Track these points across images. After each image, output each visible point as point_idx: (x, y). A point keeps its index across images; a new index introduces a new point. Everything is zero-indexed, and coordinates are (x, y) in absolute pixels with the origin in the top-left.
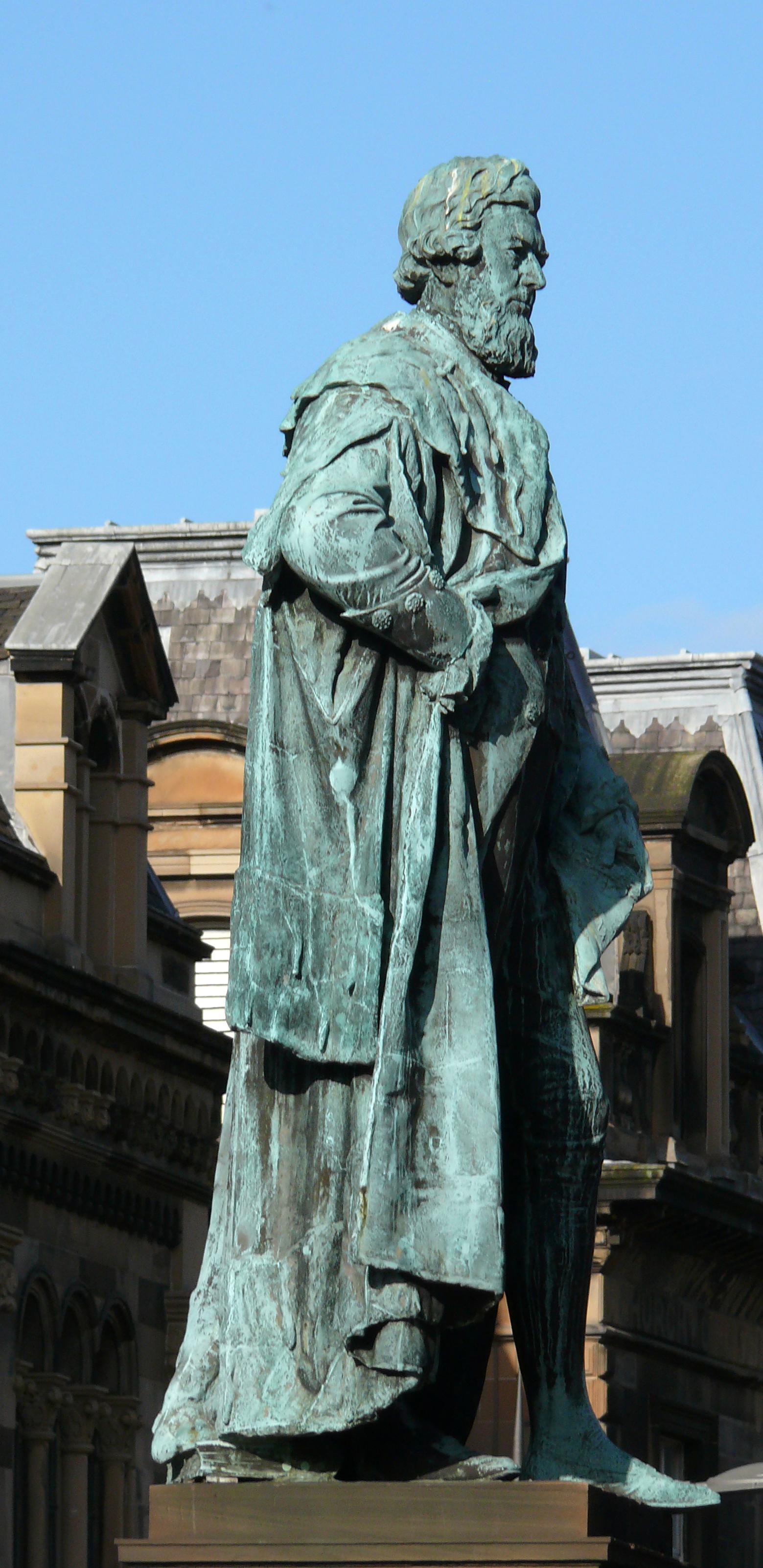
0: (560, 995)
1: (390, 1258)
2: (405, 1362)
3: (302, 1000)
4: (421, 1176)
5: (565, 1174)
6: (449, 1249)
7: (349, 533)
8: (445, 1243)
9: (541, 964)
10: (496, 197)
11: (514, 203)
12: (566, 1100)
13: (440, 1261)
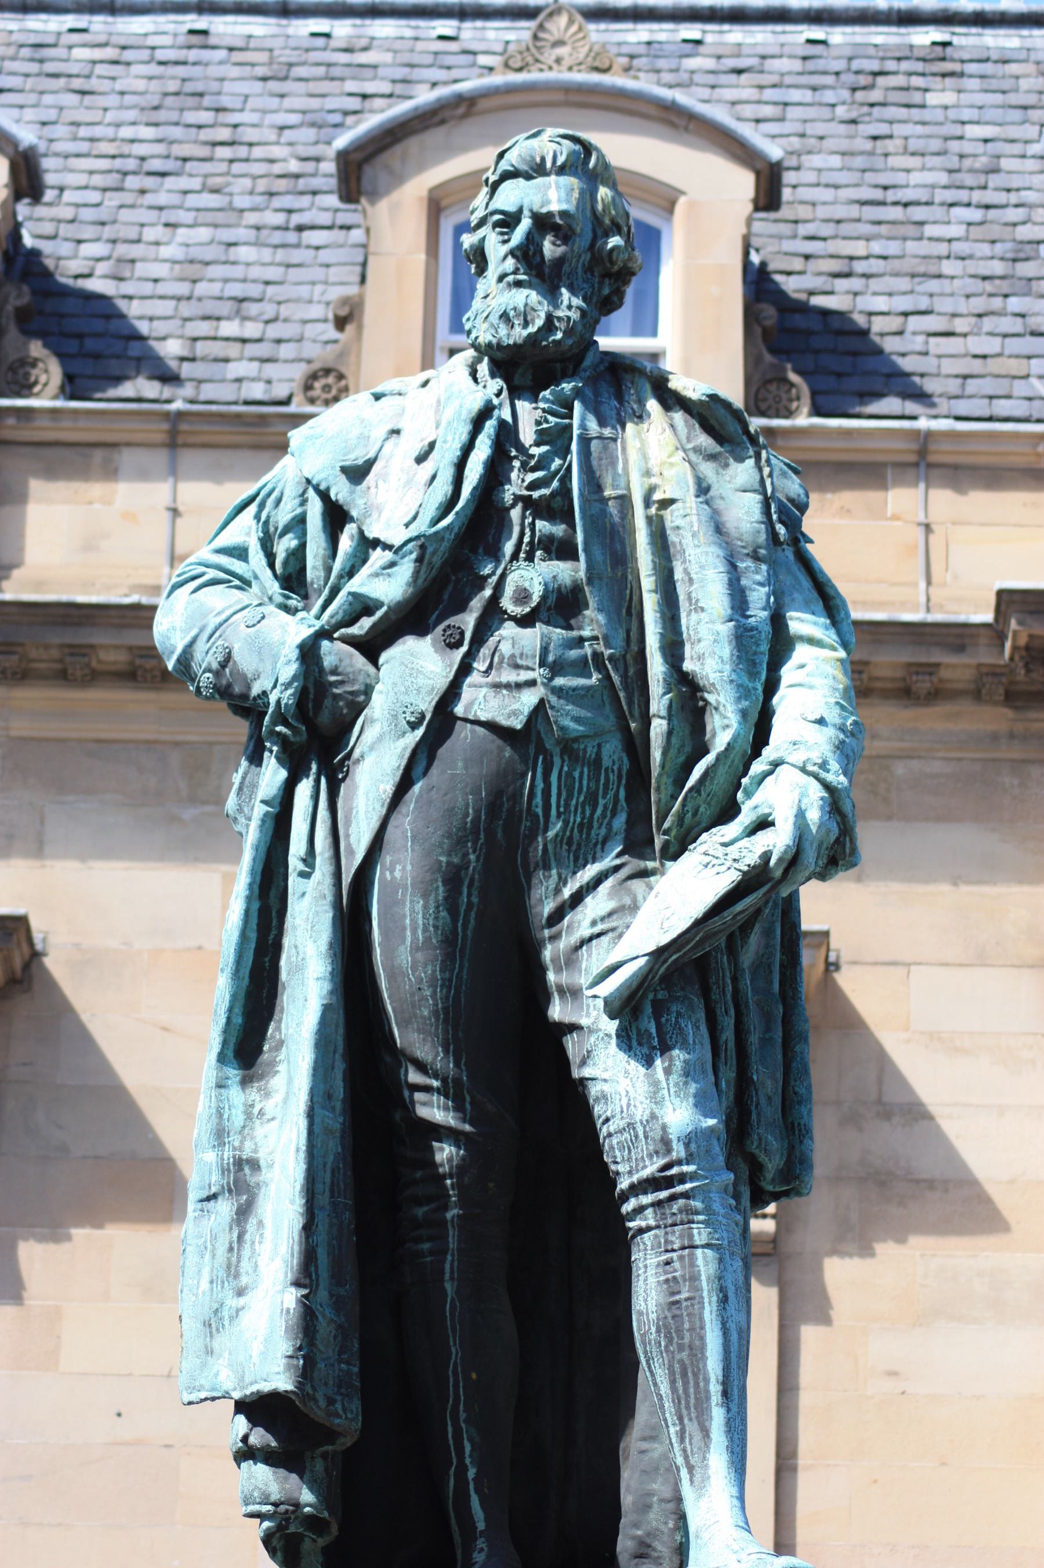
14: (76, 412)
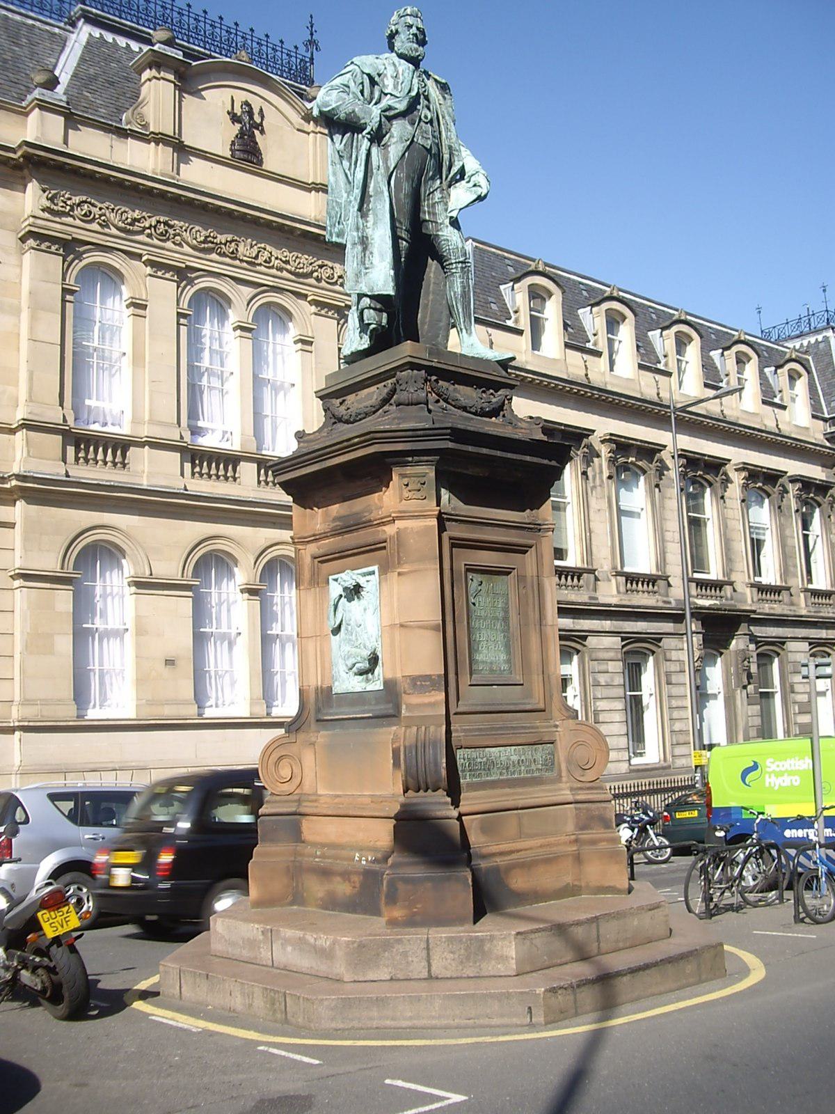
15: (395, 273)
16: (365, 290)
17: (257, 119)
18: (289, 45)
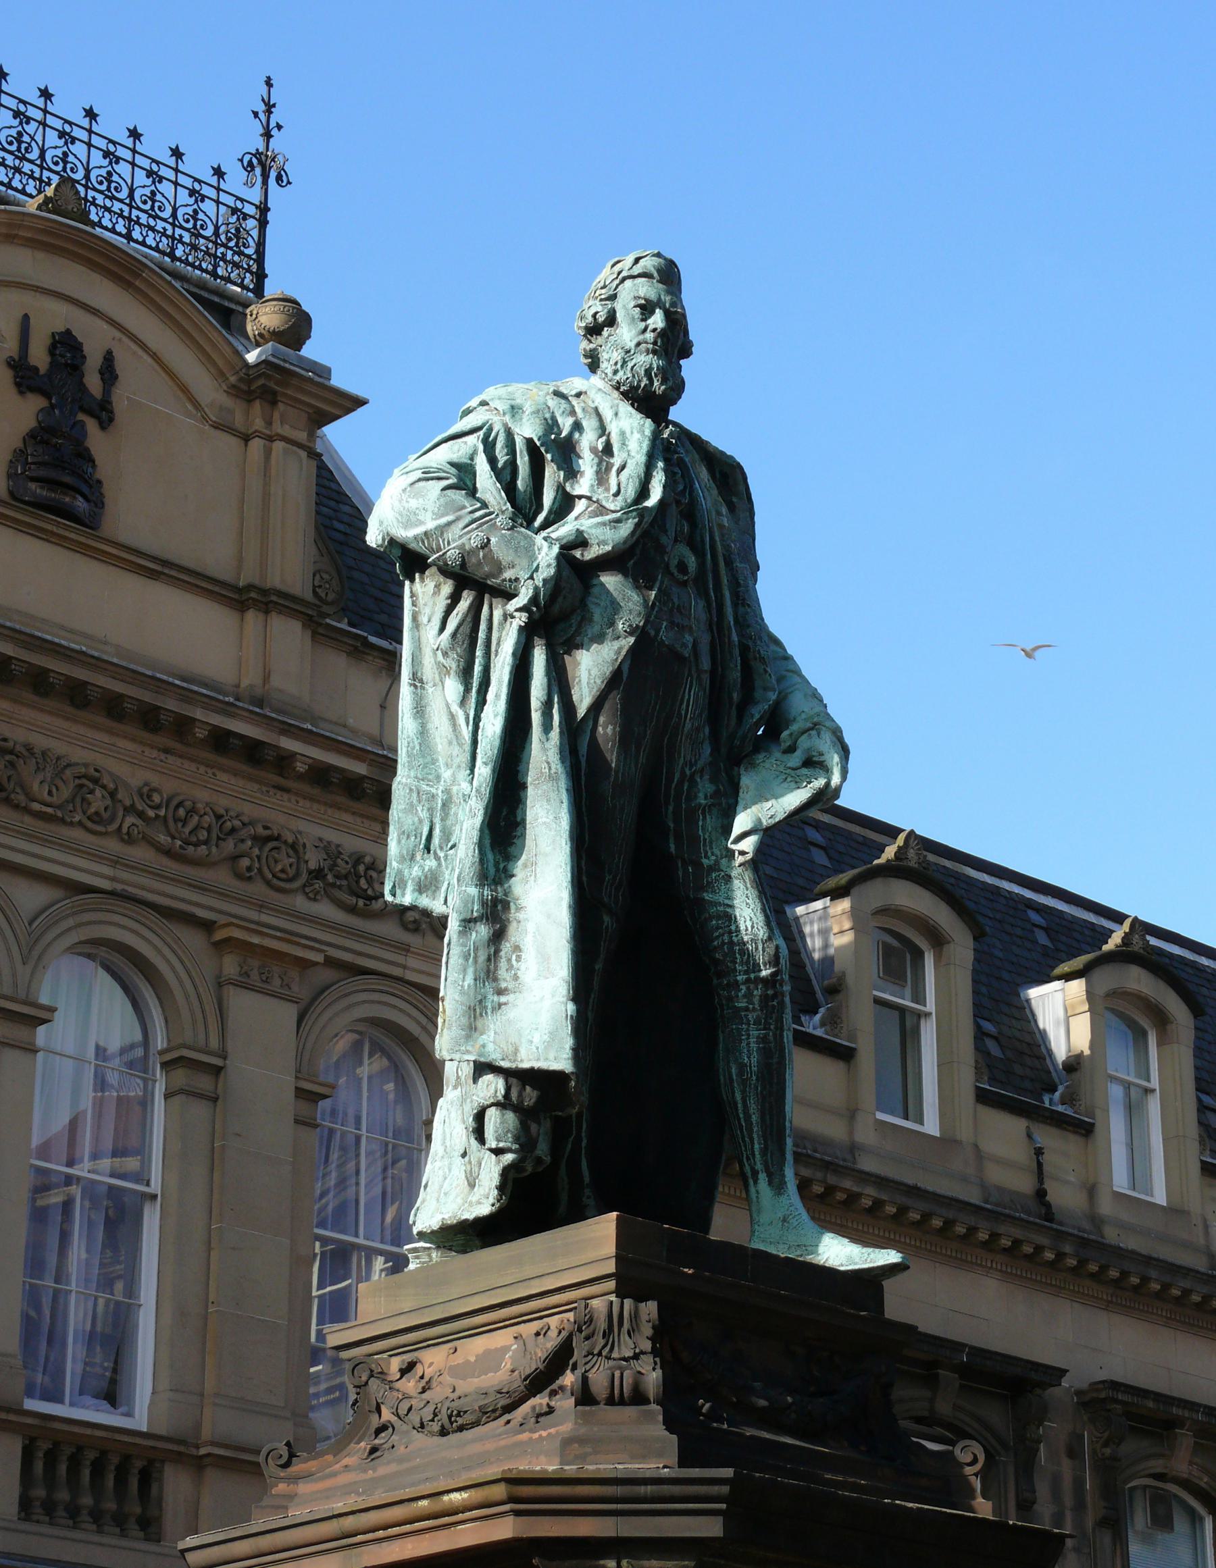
0: (724, 861)
1: (468, 1052)
2: (498, 1140)
3: (430, 870)
4: (503, 985)
5: (742, 1004)
6: (523, 1040)
7: (417, 495)
8: (520, 1035)
9: (705, 840)
10: (624, 274)
11: (639, 276)
12: (731, 943)
13: (516, 1051)
14: (1045, 1226)
15: (578, 1011)
16: (493, 1055)
17: (93, 382)
18: (197, 165)
